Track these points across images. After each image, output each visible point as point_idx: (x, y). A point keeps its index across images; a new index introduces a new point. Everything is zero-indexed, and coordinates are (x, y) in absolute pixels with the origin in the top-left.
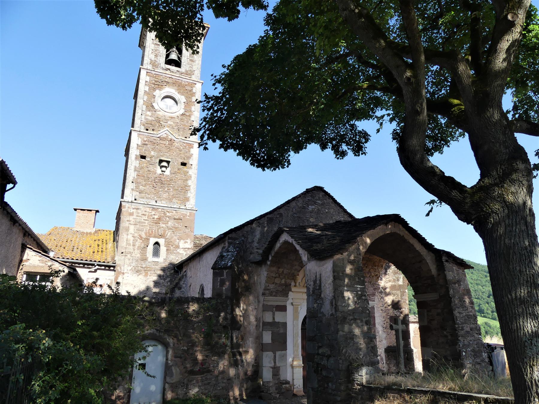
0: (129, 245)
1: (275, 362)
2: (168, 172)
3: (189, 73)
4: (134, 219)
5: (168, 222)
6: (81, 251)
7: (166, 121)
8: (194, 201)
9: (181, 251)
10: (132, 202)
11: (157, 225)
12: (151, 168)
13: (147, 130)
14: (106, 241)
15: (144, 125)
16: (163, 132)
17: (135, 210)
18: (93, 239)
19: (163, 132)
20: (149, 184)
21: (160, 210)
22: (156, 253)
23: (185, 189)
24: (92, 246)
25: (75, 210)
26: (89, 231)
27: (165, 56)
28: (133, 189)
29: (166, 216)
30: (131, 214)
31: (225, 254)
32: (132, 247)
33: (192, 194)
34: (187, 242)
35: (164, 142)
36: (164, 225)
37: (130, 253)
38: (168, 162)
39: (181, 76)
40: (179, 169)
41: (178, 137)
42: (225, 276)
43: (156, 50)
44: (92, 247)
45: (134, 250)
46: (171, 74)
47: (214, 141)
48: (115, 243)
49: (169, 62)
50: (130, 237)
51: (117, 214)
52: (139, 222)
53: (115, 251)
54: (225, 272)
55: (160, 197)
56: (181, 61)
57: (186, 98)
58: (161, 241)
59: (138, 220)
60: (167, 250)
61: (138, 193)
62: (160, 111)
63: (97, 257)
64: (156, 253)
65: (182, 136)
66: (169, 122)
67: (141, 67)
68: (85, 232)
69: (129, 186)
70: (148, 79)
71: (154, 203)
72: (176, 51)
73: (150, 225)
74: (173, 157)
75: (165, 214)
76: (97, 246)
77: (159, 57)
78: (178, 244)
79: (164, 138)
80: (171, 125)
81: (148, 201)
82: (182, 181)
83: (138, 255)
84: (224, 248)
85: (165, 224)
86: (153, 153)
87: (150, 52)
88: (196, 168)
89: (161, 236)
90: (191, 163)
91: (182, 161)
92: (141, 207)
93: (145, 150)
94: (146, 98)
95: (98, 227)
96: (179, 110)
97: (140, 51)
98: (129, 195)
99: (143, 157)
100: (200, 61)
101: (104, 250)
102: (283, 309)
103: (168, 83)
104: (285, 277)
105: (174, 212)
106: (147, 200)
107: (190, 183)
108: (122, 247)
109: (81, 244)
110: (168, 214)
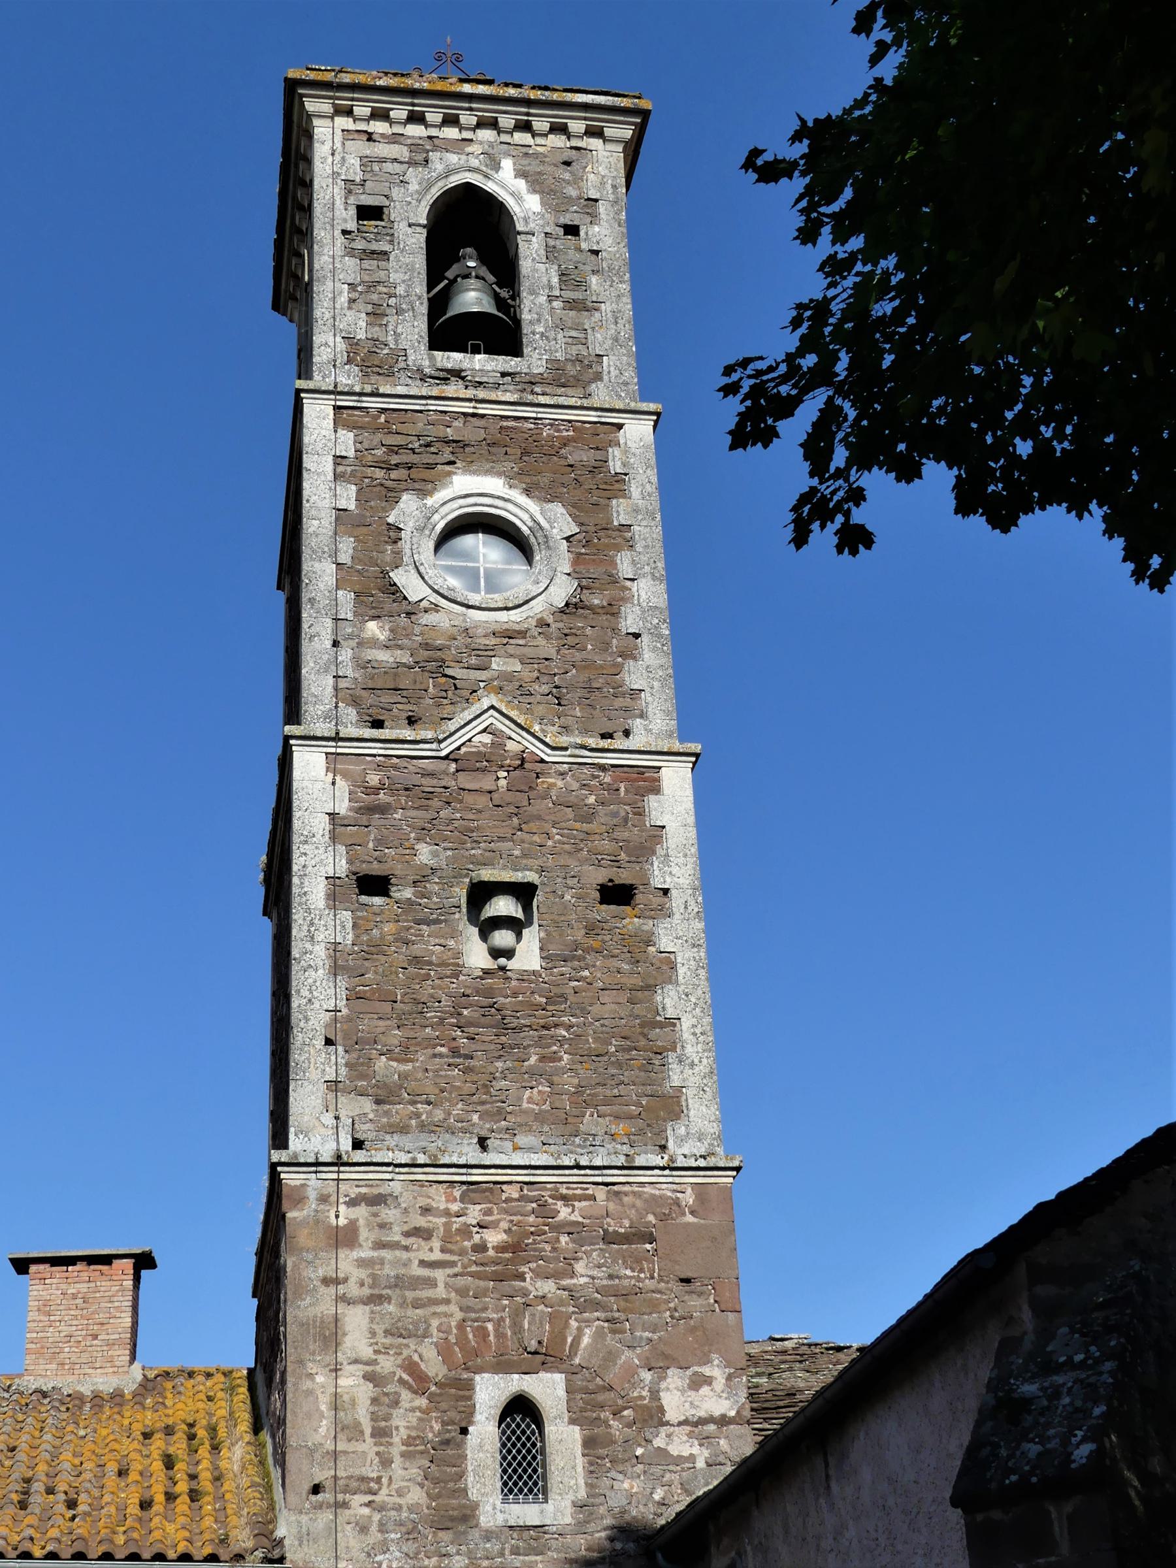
0: (354, 1431)
2: (528, 954)
3: (575, 374)
4: (361, 1263)
5: (570, 1260)
6: (72, 1504)
7: (481, 657)
8: (714, 1111)
9: (681, 1445)
10: (339, 1161)
11: (506, 1286)
12: (429, 944)
13: (378, 724)
14: (213, 1430)
15: (355, 702)
16: (472, 726)
17: (361, 1213)
18: (138, 1428)
19: (472, 726)
20: (431, 1043)
21: (513, 1192)
22: (524, 1471)
23: (651, 1040)
24: (136, 1467)
25: (21, 1266)
26: (105, 1382)
27: (423, 309)
28: (334, 1085)
29: (559, 1228)
30: (345, 1237)
31: (1030, 1389)
32: (368, 1446)
33: (692, 1070)
34: (708, 1381)
35: (487, 783)
36: (548, 1287)
37: (367, 1486)
38: (524, 893)
39: (530, 398)
40: (591, 929)
41: (564, 740)
42: (1065, 1548)
43: (372, 286)
44: (133, 1476)
45: (386, 1462)
46: (470, 393)
47: (908, 472)
48: (265, 1436)
49: (448, 332)
50: (351, 1381)
51: (260, 1254)
52: (399, 1283)
53: (269, 1488)
54: (1058, 1515)
55: (501, 1115)
56: (517, 322)
57: (576, 510)
58: (548, 1389)
59: (389, 1271)
60: (589, 1443)
61: (367, 1105)
62: (436, 608)
63: (170, 1528)
64: (524, 1471)
65: (586, 732)
66: (496, 664)
67: (300, 384)
68: (86, 1390)
69: (314, 1066)
70: (347, 442)
71: (472, 1154)
72: (484, 271)
73: (462, 1292)
74: (550, 862)
75: (544, 1211)
76: (158, 1465)
77: (392, 319)
78: (655, 1394)
79: (480, 756)
80: (508, 677)
81: (434, 1143)
82: (623, 997)
83: (416, 1495)
84: (1007, 1346)
85: (556, 1275)
86: (425, 854)
87: (343, 299)
88: (694, 908)
89: (543, 1358)
90: (657, 882)
91: (601, 876)
92: (396, 1187)
93: (379, 842)
94: (347, 549)
95: (159, 1353)
96: (549, 586)
97: (288, 330)
98: (316, 1129)
99: (373, 884)
100: (627, 300)
101: (205, 1482)
103: (459, 445)
105: (601, 1193)
106: (424, 1140)
107: (669, 1001)
108: (312, 1451)
109: (67, 1459)
110: (564, 1213)
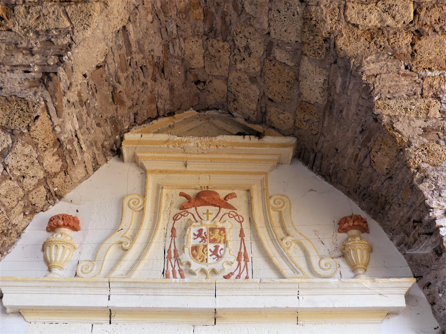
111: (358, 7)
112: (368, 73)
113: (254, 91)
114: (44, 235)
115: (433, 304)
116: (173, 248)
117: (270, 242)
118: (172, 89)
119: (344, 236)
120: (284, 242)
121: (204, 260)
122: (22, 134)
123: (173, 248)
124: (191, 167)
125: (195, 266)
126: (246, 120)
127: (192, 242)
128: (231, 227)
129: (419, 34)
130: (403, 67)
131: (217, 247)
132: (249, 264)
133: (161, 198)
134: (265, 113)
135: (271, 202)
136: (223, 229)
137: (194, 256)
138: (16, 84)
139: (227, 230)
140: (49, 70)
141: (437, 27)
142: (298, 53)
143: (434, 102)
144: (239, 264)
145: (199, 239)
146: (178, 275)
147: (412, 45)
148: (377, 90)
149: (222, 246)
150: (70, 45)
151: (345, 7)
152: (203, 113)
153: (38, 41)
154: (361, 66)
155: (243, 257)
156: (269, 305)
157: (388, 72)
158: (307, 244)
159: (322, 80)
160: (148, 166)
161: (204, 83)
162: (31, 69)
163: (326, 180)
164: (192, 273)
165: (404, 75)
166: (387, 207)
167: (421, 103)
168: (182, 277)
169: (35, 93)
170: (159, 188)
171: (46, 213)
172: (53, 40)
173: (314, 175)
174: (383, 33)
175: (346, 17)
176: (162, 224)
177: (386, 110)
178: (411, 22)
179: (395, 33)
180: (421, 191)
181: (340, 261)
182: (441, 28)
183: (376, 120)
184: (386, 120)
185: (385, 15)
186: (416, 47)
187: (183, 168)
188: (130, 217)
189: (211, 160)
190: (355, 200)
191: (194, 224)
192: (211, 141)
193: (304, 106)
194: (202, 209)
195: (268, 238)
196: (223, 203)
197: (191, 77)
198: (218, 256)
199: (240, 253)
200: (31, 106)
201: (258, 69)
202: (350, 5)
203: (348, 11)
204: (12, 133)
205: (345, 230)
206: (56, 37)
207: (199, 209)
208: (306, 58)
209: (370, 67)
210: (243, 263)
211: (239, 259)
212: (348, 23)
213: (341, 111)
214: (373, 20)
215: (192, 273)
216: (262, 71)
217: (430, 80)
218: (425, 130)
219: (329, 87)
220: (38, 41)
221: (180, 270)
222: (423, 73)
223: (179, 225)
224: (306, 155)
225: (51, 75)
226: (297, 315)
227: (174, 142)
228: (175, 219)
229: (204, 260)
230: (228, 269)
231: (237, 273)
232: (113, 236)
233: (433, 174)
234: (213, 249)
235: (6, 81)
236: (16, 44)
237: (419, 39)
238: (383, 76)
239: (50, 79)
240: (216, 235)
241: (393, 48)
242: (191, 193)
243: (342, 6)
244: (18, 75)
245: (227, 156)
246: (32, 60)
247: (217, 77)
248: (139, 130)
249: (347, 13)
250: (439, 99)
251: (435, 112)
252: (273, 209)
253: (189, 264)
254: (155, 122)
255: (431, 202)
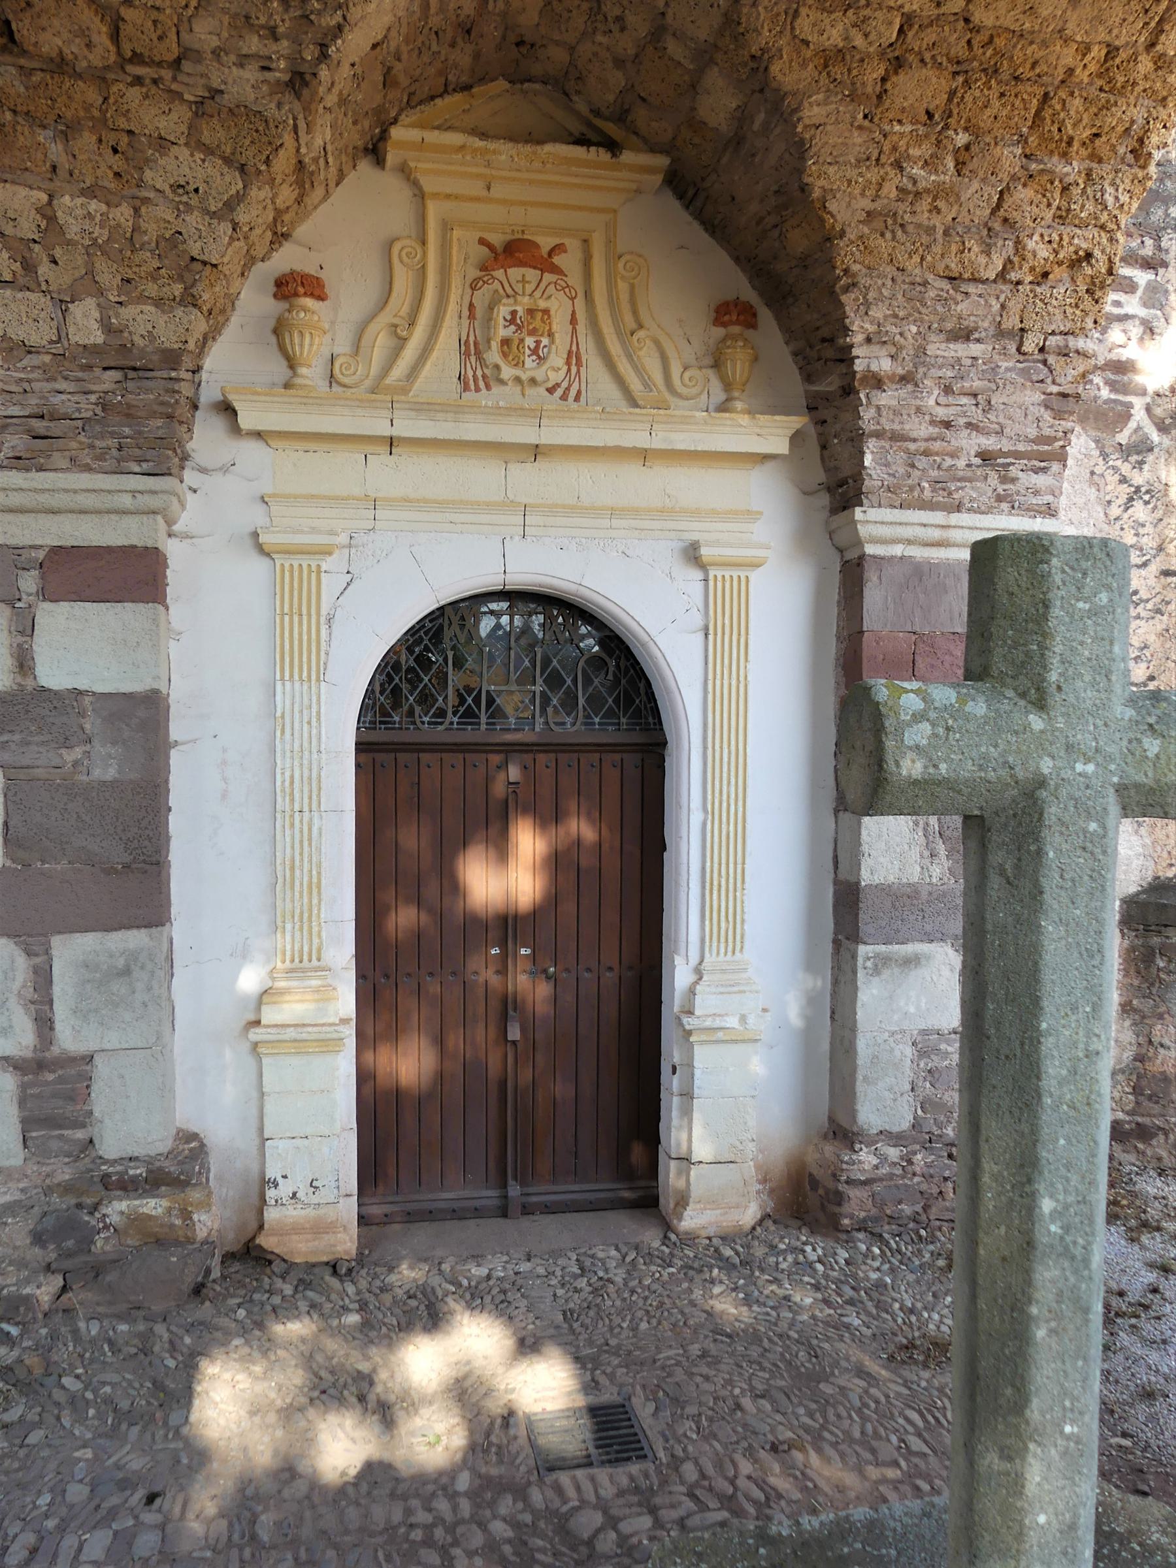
1: (44, 1024)
102: (133, 576)
104: (89, 284)
111: (815, 15)
112: (807, 121)
113: (617, 79)
114: (271, 306)
115: (824, 447)
116: (472, 339)
117: (614, 337)
118: (477, 56)
119: (720, 332)
120: (635, 338)
121: (519, 364)
122: (260, 172)
123: (472, 339)
124: (497, 191)
125: (507, 372)
126: (591, 111)
127: (502, 332)
128: (558, 307)
129: (898, 64)
130: (861, 116)
131: (538, 343)
132: (583, 370)
133: (451, 247)
134: (627, 111)
135: (621, 265)
136: (546, 312)
137: (505, 355)
138: (249, 89)
139: (552, 313)
140: (304, 68)
141: (927, 57)
142: (706, 56)
143: (892, 173)
144: (569, 370)
145: (513, 328)
146: (481, 384)
147: (884, 80)
148: (814, 150)
149: (545, 341)
150: (340, 28)
151: (796, 14)
152: (518, 86)
153: (286, 17)
154: (796, 110)
155: (574, 358)
156: (611, 444)
157: (837, 122)
158: (663, 339)
159: (734, 105)
160: (429, 184)
161: (532, 45)
162: (274, 65)
163: (706, 230)
164: (502, 382)
165: (860, 128)
166: (790, 300)
167: (873, 175)
168: (488, 387)
169: (279, 105)
170: (446, 227)
171: (267, 263)
172: (312, 17)
173: (690, 219)
174: (844, 59)
175: (793, 28)
176: (454, 297)
177: (823, 176)
178: (891, 45)
179: (862, 60)
180: (841, 305)
181: (710, 373)
182: (933, 57)
183: (803, 190)
184: (816, 193)
185: (853, 32)
186: (888, 86)
187: (484, 193)
188: (403, 281)
189: (531, 182)
190: (744, 271)
191: (504, 301)
192: (535, 153)
193: (696, 125)
194: (515, 273)
195: (612, 330)
196: (546, 264)
197: (512, 38)
198: (539, 357)
199: (570, 352)
200: (271, 125)
201: (631, 52)
202: (804, 11)
203: (799, 21)
204: (242, 168)
205: (724, 325)
206: (319, 13)
207: (510, 271)
208: (716, 69)
209: (812, 112)
210: (574, 369)
211: (568, 363)
212: (795, 37)
213: (753, 155)
214: (834, 36)
215: (502, 382)
216: (637, 56)
217: (895, 138)
218: (869, 213)
219: (742, 117)
220: (286, 17)
221: (484, 376)
222: (887, 128)
223: (481, 298)
224: (682, 184)
225: (308, 77)
226: (644, 455)
227: (475, 150)
228: (473, 288)
229: (519, 364)
230: (554, 378)
231: (565, 385)
232: (382, 314)
233: (863, 281)
234: (533, 346)
235: (230, 81)
236: (247, 17)
237: (896, 73)
238: (829, 128)
239: (306, 84)
240: (534, 320)
241: (853, 84)
242: (497, 239)
243: (791, 12)
244: (251, 74)
245: (557, 178)
246: (275, 48)
247: (557, 43)
248: (414, 118)
249: (796, 24)
250: (901, 169)
251: (890, 190)
252: (623, 277)
253: (497, 367)
254: (438, 101)
255: (852, 323)
